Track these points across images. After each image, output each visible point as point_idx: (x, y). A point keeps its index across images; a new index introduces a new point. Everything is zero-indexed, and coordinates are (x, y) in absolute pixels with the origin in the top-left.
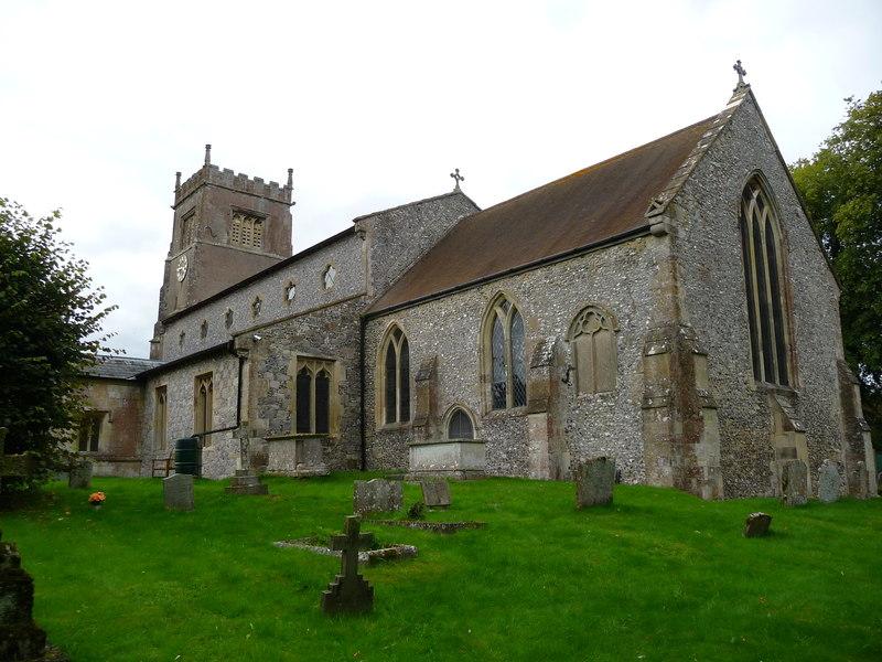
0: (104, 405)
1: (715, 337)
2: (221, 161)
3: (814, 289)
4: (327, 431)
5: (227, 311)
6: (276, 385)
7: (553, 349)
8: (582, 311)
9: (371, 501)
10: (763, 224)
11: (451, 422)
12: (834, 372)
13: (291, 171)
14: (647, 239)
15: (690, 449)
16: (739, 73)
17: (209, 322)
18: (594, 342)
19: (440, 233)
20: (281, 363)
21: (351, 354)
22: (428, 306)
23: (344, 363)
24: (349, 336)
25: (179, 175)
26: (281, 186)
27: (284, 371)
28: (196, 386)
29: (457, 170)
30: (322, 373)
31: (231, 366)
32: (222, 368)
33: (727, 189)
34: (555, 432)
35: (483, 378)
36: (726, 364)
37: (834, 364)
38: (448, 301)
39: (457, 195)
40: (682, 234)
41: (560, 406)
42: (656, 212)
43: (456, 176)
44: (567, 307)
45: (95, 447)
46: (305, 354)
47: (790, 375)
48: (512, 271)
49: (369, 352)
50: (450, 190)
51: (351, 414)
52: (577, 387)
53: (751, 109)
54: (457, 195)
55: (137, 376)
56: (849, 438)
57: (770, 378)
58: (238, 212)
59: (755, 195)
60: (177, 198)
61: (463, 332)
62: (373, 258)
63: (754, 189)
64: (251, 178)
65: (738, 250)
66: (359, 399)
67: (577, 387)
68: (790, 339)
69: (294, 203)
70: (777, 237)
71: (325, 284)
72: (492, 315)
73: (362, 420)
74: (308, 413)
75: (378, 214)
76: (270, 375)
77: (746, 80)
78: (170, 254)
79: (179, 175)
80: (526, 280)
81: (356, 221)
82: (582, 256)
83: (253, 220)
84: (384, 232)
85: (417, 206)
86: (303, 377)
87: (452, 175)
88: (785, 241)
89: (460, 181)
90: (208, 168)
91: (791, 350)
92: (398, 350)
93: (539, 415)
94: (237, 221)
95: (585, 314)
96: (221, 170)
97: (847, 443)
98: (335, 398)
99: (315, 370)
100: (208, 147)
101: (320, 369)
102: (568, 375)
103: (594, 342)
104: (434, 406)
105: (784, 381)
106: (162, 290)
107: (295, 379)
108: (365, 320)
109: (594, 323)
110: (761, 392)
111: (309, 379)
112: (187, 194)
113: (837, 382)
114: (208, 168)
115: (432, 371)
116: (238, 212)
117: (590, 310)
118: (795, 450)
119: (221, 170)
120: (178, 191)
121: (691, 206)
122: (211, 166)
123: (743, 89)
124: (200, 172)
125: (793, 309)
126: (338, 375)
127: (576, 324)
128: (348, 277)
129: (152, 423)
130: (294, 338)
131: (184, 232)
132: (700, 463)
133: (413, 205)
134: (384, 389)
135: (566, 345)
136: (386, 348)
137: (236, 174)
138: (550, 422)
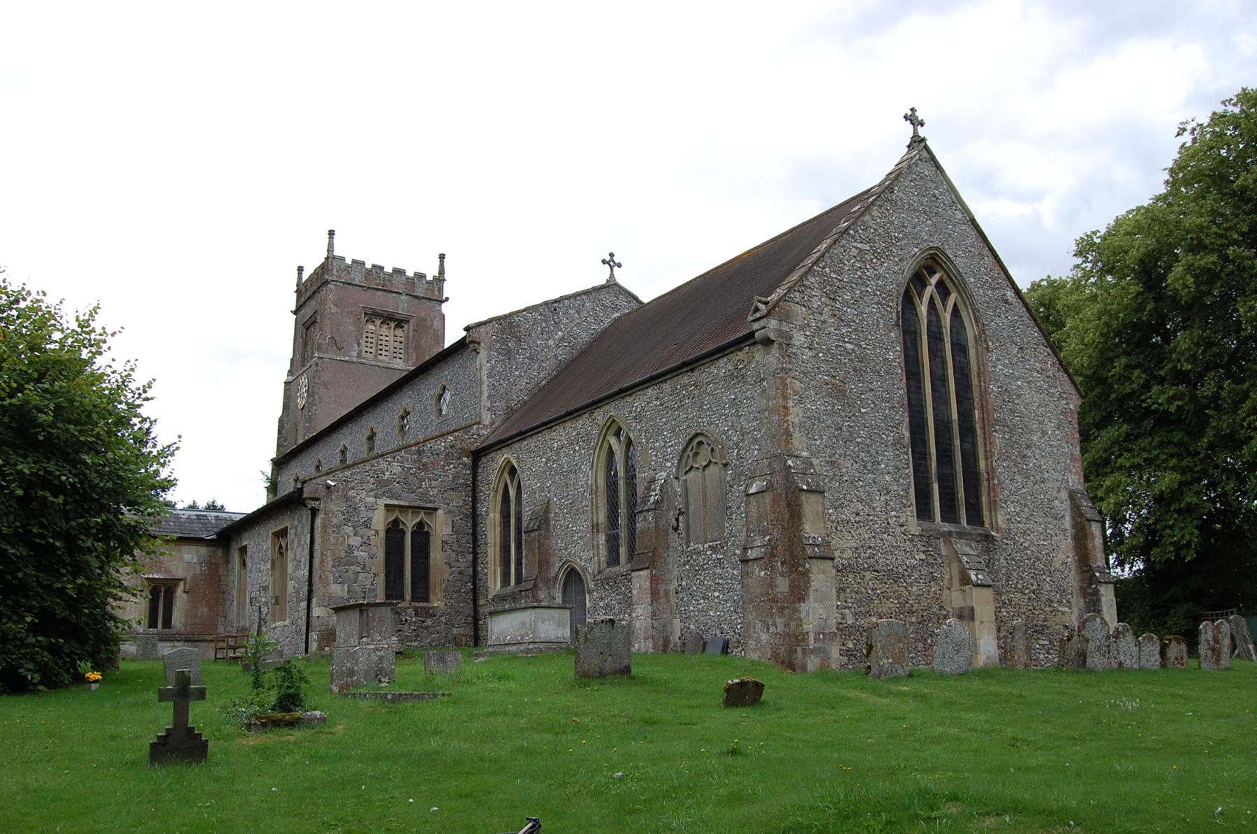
0: (178, 572)
1: (826, 471)
2: (347, 251)
3: (1032, 398)
4: (427, 599)
5: (341, 447)
6: (355, 541)
7: (662, 486)
8: (691, 440)
9: (351, 673)
10: (946, 318)
11: (565, 584)
12: (1063, 505)
13: (442, 257)
14: (755, 348)
15: (796, 610)
16: (912, 123)
17: (323, 461)
18: (704, 479)
19: (584, 337)
20: (364, 514)
21: (459, 500)
22: (540, 437)
23: (449, 512)
24: (456, 477)
25: (300, 269)
26: (430, 278)
27: (367, 524)
28: (274, 545)
29: (612, 255)
30: (421, 525)
31: (305, 517)
32: (296, 523)
33: (878, 277)
34: (662, 593)
35: (595, 527)
36: (869, 502)
37: (1064, 495)
38: (560, 429)
39: (612, 286)
40: (799, 339)
41: (670, 560)
42: (758, 315)
43: (611, 262)
44: (677, 435)
45: (167, 623)
46: (395, 502)
47: (986, 513)
48: (622, 391)
49: (481, 496)
50: (602, 281)
51: (459, 577)
52: (688, 536)
53: (928, 170)
54: (612, 286)
55: (218, 534)
56: (1083, 592)
57: (949, 513)
58: (372, 315)
59: (934, 280)
60: (298, 300)
61: (575, 470)
62: (489, 376)
63: (932, 272)
64: (388, 269)
65: (895, 355)
66: (470, 557)
67: (688, 536)
68: (987, 465)
69: (447, 299)
70: (970, 332)
71: (440, 410)
72: (606, 446)
73: (474, 584)
74: (402, 577)
75: (498, 319)
76: (349, 530)
77: (922, 132)
78: (290, 373)
79: (300, 269)
80: (638, 402)
81: (467, 329)
82: (692, 370)
83: (393, 325)
84: (505, 342)
85: (552, 306)
86: (394, 532)
87: (604, 262)
88: (981, 338)
89: (616, 269)
90: (331, 259)
91: (988, 480)
92: (512, 493)
93: (641, 573)
94: (371, 327)
95: (695, 442)
96: (349, 261)
97: (1082, 600)
98: (437, 556)
99: (410, 522)
100: (331, 233)
101: (418, 520)
102: (677, 520)
103: (704, 479)
104: (544, 564)
105: (975, 516)
106: (281, 421)
107: (382, 534)
108: (478, 455)
109: (705, 452)
110: (928, 538)
111: (403, 532)
112: (308, 294)
113: (1068, 518)
114: (331, 259)
115: (543, 521)
116: (372, 315)
117: (700, 438)
118: (972, 609)
119: (349, 261)
120: (299, 292)
121: (816, 303)
122: (334, 257)
123: (918, 142)
124: (322, 267)
125: (993, 426)
126: (441, 527)
127: (685, 455)
128: (462, 401)
129: (235, 593)
130: (381, 483)
131: (306, 344)
132: (806, 628)
133: (546, 304)
134: (498, 544)
135: (676, 483)
136: (501, 491)
137: (369, 266)
138: (654, 580)
